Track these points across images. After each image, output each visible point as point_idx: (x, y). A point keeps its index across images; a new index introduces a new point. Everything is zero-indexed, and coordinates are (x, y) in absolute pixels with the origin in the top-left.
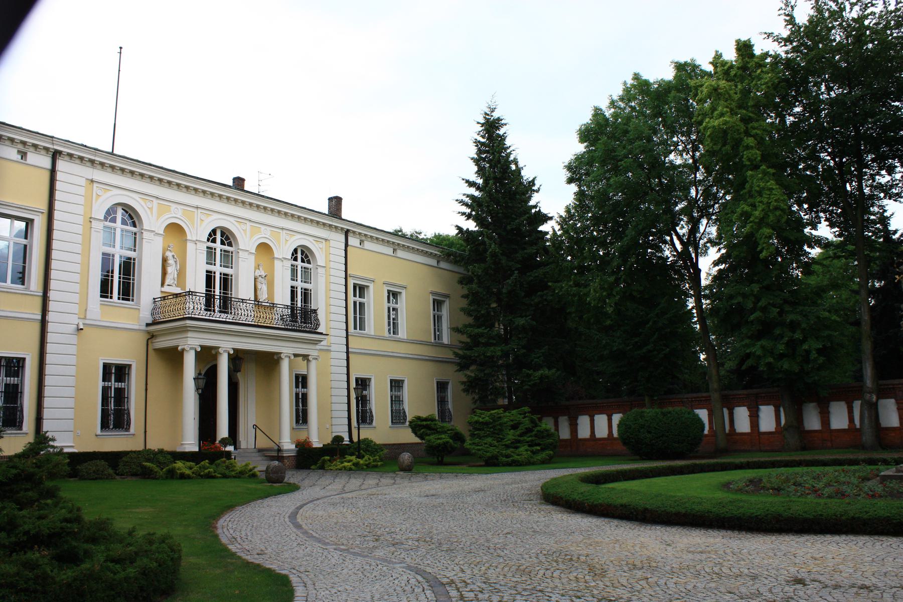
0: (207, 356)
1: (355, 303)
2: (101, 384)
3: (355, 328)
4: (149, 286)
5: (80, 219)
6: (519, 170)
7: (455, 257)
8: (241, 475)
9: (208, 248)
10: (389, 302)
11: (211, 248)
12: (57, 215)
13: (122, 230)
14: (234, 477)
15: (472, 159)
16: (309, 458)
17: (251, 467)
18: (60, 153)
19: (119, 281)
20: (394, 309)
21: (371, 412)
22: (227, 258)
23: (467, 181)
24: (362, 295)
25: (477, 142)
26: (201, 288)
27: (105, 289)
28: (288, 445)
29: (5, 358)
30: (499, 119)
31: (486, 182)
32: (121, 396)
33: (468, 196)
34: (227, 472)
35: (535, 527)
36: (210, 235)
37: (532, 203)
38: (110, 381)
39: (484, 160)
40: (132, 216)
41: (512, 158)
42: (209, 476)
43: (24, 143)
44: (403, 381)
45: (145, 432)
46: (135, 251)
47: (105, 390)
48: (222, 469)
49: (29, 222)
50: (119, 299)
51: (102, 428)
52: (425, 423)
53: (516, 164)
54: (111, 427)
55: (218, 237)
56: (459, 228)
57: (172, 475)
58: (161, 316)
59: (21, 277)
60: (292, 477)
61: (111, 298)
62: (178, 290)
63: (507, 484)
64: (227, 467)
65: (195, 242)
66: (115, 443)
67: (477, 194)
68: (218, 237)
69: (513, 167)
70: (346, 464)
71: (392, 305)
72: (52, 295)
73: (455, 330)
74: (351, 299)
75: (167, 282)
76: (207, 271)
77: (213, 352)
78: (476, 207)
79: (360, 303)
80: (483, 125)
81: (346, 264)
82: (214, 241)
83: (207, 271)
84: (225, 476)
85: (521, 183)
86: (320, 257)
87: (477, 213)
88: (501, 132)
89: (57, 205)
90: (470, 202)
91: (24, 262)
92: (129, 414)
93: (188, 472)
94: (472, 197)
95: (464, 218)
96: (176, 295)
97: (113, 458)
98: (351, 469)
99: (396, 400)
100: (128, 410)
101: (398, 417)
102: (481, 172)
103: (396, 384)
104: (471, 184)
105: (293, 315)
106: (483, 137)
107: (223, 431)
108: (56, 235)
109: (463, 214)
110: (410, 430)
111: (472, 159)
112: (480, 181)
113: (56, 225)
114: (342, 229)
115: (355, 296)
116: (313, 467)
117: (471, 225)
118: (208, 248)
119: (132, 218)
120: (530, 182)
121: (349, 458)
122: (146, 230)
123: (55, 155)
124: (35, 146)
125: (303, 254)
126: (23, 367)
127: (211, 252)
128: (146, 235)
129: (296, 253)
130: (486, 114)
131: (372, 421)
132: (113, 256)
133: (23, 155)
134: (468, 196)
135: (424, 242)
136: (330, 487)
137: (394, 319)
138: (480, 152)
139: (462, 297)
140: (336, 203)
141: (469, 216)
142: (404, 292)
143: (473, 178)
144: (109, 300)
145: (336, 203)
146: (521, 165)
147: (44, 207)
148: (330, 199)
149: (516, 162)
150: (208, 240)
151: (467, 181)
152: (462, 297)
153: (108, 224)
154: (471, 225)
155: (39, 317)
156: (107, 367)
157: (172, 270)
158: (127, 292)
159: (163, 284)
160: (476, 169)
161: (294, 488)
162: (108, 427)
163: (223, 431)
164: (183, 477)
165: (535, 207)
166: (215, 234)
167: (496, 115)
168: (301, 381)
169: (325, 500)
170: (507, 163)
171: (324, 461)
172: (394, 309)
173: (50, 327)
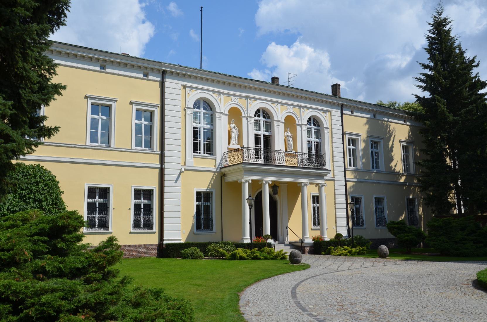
0: (256, 185)
1: (349, 150)
2: (196, 203)
3: (350, 165)
4: (221, 145)
5: (181, 109)
6: (462, 53)
7: (416, 116)
8: (275, 258)
9: (255, 120)
10: (372, 148)
11: (257, 121)
12: (167, 107)
13: (204, 114)
14: (272, 259)
15: (426, 49)
16: (320, 247)
17: (283, 252)
18: (166, 71)
19: (202, 143)
20: (376, 153)
21: (362, 219)
22: (268, 126)
23: (423, 65)
24: (377, 148)
25: (429, 38)
26: (252, 144)
27: (196, 147)
28: (309, 240)
29: (143, 190)
30: (445, 20)
31: (436, 64)
32: (208, 210)
33: (424, 75)
34: (268, 256)
35: (465, 308)
36: (256, 112)
37: (473, 75)
38: (200, 201)
39: (434, 49)
40: (208, 106)
41: (456, 44)
42: (256, 258)
43: (146, 68)
44: (383, 199)
45: (222, 231)
46: (200, 123)
47: (198, 207)
48: (265, 254)
49: (152, 113)
50: (204, 153)
51: (197, 229)
52: (397, 226)
53: (460, 49)
54: (202, 228)
55: (261, 114)
56: (417, 96)
57: (234, 257)
58: (228, 162)
59: (149, 144)
60: (305, 259)
61: (200, 153)
62: (238, 147)
63: (453, 270)
64: (268, 253)
65: (301, 126)
66: (204, 237)
67: (430, 73)
68: (261, 114)
69: (457, 51)
70: (344, 251)
71: (374, 150)
72: (166, 153)
73: (417, 164)
74: (347, 147)
75: (233, 141)
76: (255, 135)
77: (260, 183)
78: (429, 83)
79: (353, 150)
80: (433, 25)
81: (342, 125)
82: (259, 116)
83: (255, 135)
84: (266, 258)
85: (464, 62)
86: (326, 123)
87: (431, 86)
88: (447, 28)
89: (167, 101)
90: (423, 77)
91: (151, 135)
92: (212, 220)
93: (244, 255)
94: (426, 75)
95: (421, 90)
96: (236, 150)
97: (203, 247)
98: (346, 255)
99: (379, 211)
100: (212, 218)
101: (380, 221)
102: (432, 58)
103: (379, 201)
104: (426, 67)
105: (310, 160)
106: (433, 34)
107: (267, 230)
108: (167, 118)
109: (421, 87)
110: (387, 230)
111: (426, 49)
112: (432, 64)
113: (167, 113)
114: (338, 104)
115: (349, 145)
116: (323, 253)
117: (427, 95)
118: (255, 120)
119: (209, 106)
120: (470, 61)
121: (346, 247)
122: (218, 112)
123: (164, 73)
124: (152, 69)
125: (314, 121)
126: (152, 194)
127: (309, 131)
128: (218, 115)
129: (310, 120)
130: (435, 17)
131: (363, 224)
132: (200, 129)
133: (146, 75)
134: (424, 75)
135: (397, 110)
136: (329, 267)
137: (376, 159)
138: (431, 44)
139: (423, 142)
140: (336, 88)
141: (425, 89)
142: (382, 141)
143: (427, 62)
144: (198, 154)
145: (336, 88)
146: (463, 49)
147: (158, 102)
148: (333, 86)
149: (459, 47)
150: (255, 116)
151: (423, 65)
152: (423, 142)
153: (195, 110)
154: (427, 95)
155: (159, 166)
156: (199, 194)
157: (234, 135)
158: (209, 149)
159: (229, 143)
160: (428, 56)
161: (306, 267)
162: (201, 228)
163: (267, 230)
164: (241, 258)
165: (476, 77)
166: (259, 112)
167: (443, 17)
168: (316, 199)
169: (321, 276)
170: (451, 49)
171: (330, 249)
172: (376, 153)
173: (166, 172)
